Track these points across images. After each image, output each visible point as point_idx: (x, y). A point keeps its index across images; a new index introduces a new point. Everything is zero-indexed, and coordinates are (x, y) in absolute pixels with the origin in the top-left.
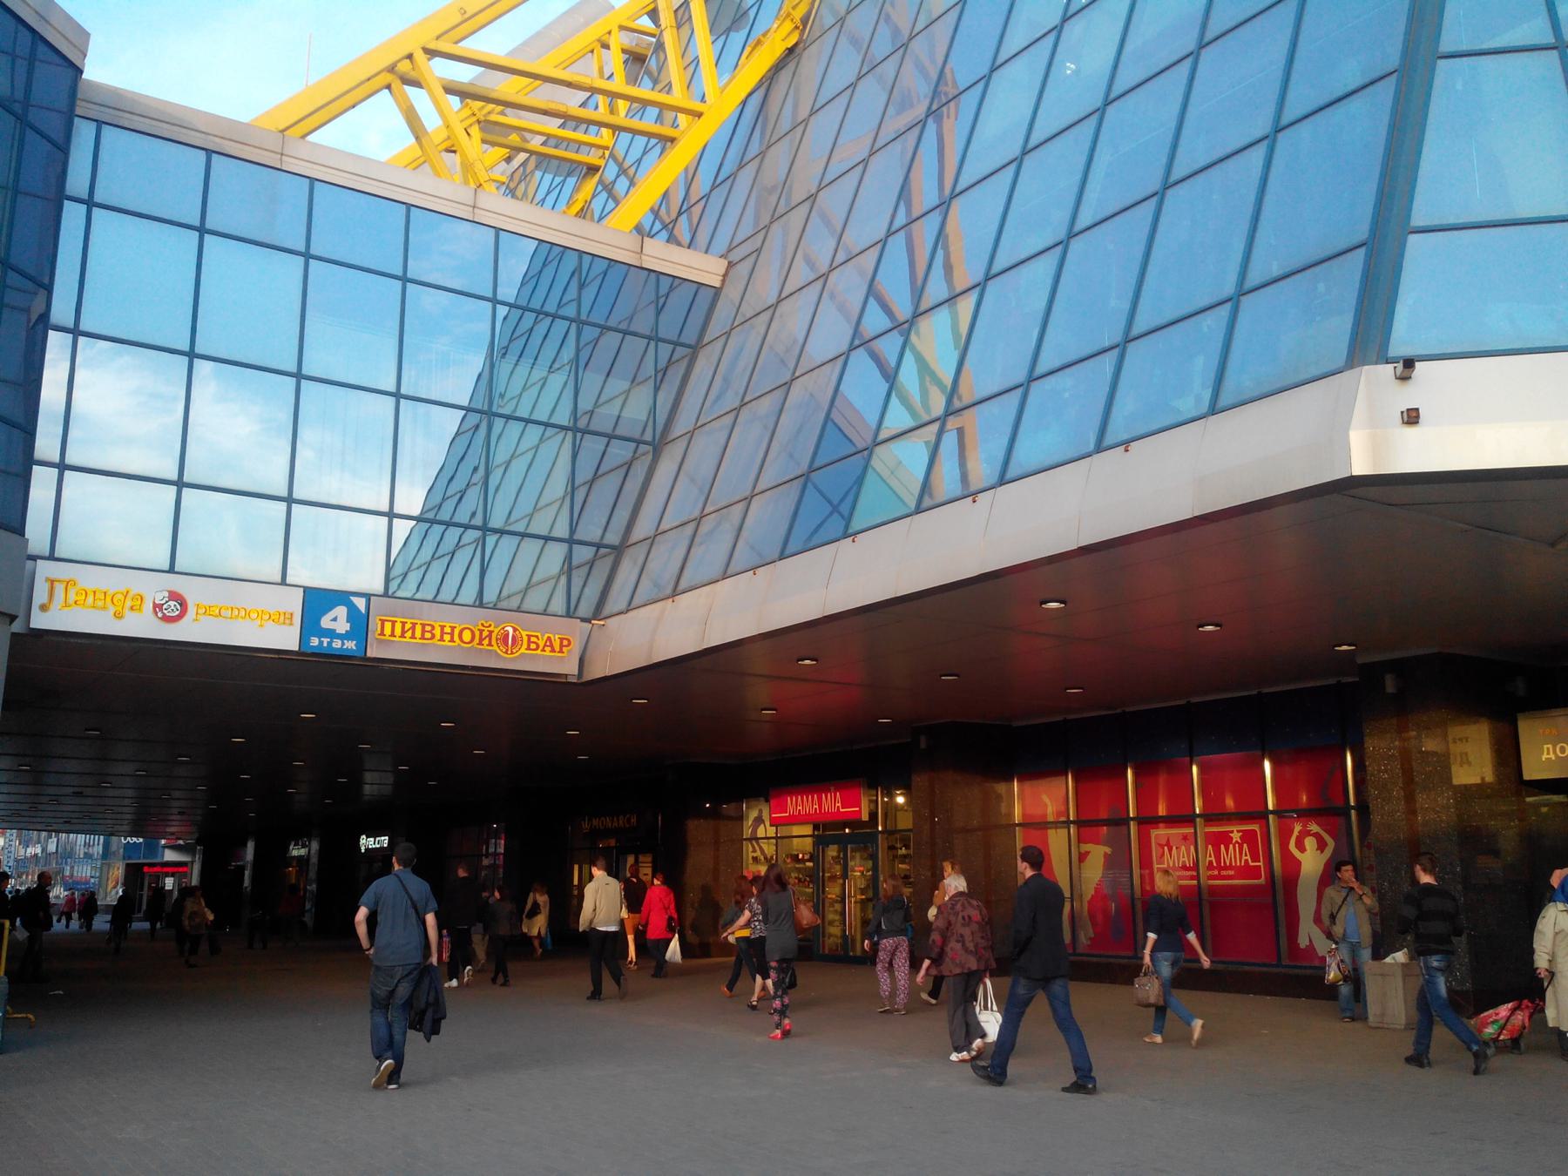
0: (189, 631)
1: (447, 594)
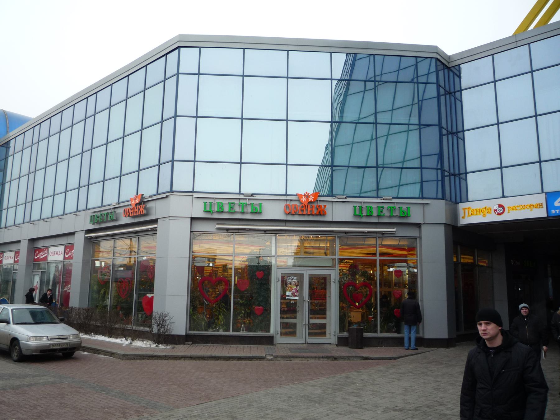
0: (507, 217)
1: (27, 219)
